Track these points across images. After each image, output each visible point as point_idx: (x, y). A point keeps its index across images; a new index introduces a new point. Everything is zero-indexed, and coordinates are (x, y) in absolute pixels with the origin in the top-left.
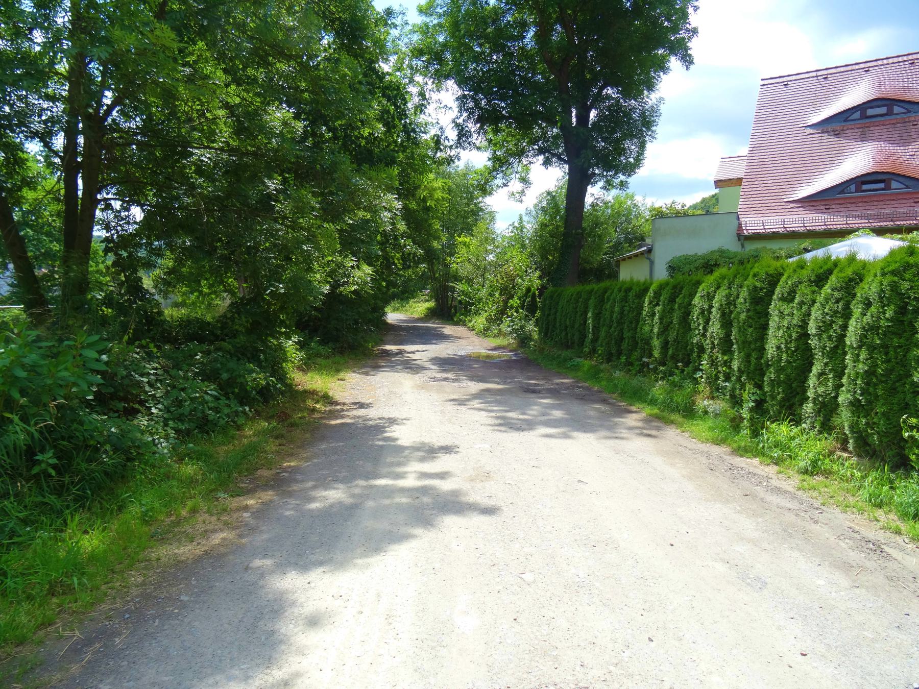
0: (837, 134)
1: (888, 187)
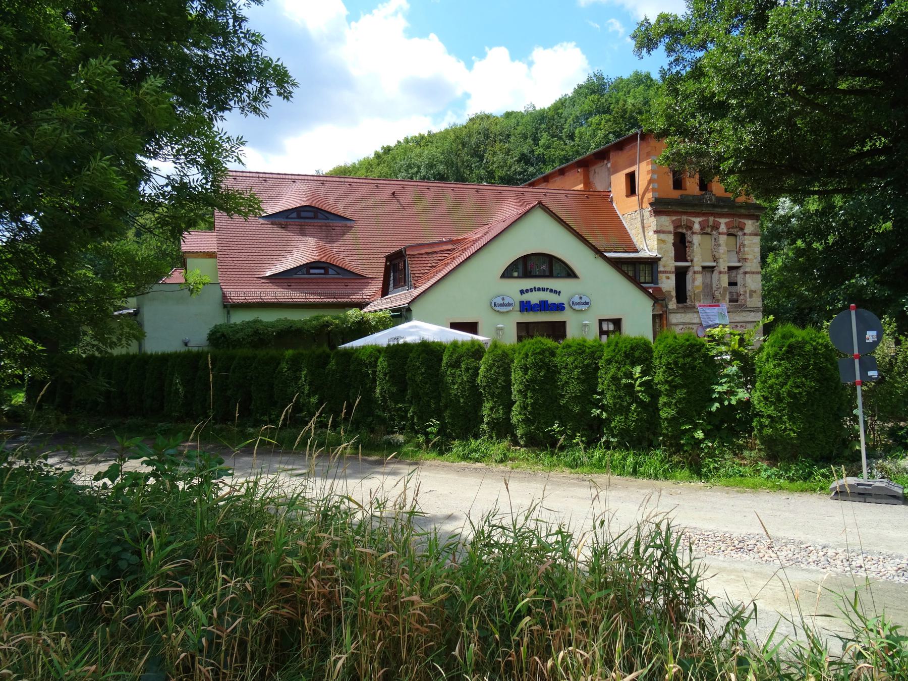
0: (284, 227)
1: (326, 273)
